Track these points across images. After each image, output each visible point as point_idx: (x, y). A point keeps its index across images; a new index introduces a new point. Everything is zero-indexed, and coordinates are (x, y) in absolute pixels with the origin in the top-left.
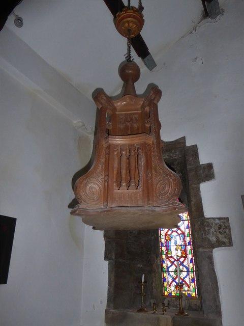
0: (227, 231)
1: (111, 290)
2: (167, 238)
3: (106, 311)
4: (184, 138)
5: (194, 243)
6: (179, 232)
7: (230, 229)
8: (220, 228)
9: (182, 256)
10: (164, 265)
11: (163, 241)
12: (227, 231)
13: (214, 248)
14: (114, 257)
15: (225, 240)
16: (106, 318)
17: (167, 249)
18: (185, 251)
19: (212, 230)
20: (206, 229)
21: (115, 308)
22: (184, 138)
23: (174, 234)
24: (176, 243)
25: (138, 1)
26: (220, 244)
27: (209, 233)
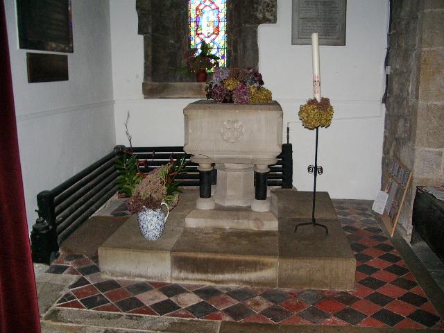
0: (274, 9)
1: (148, 64)
2: (198, 13)
3: (143, 84)
4: (372, 202)
5: (229, 17)
6: (213, 7)
7: (276, 8)
8: (268, 6)
9: (213, 33)
10: (192, 42)
11: (193, 16)
12: (274, 9)
13: (259, 24)
14: (150, 30)
15: (271, 18)
16: (144, 89)
17: (197, 25)
18: (218, 27)
19: (261, 7)
20: (255, 6)
21: (154, 80)
22: (372, 202)
23: (207, 9)
24: (208, 18)
25: (291, 1)
26: (266, 20)
27: (257, 10)
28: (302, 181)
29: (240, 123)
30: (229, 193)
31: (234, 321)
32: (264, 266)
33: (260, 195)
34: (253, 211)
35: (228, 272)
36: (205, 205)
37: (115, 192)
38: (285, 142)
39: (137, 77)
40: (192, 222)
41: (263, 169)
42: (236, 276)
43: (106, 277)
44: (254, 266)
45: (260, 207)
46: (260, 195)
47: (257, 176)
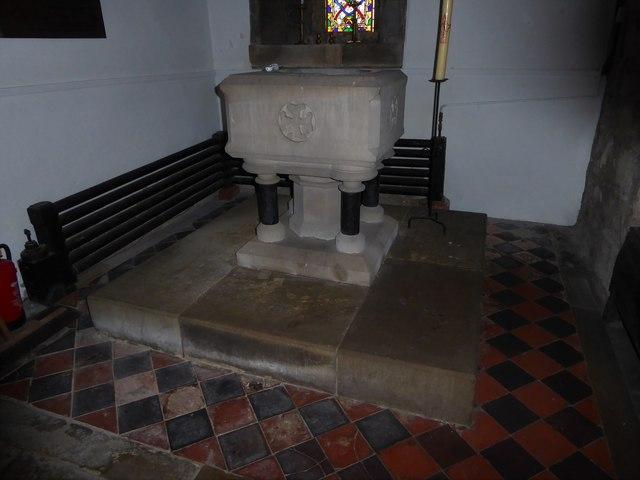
16: (251, 56)
28: (462, 191)
29: (308, 109)
30: (308, 217)
31: (548, 260)
32: (316, 360)
33: (350, 224)
34: (339, 253)
35: (261, 358)
36: (271, 235)
37: (215, 190)
38: (418, 128)
39: (242, 37)
40: (246, 260)
41: (354, 187)
42: (274, 367)
43: (99, 338)
44: (302, 358)
45: (349, 246)
46: (350, 224)
47: (345, 196)
